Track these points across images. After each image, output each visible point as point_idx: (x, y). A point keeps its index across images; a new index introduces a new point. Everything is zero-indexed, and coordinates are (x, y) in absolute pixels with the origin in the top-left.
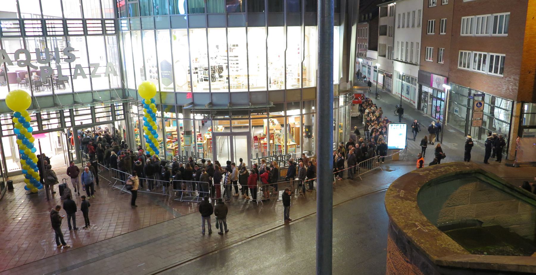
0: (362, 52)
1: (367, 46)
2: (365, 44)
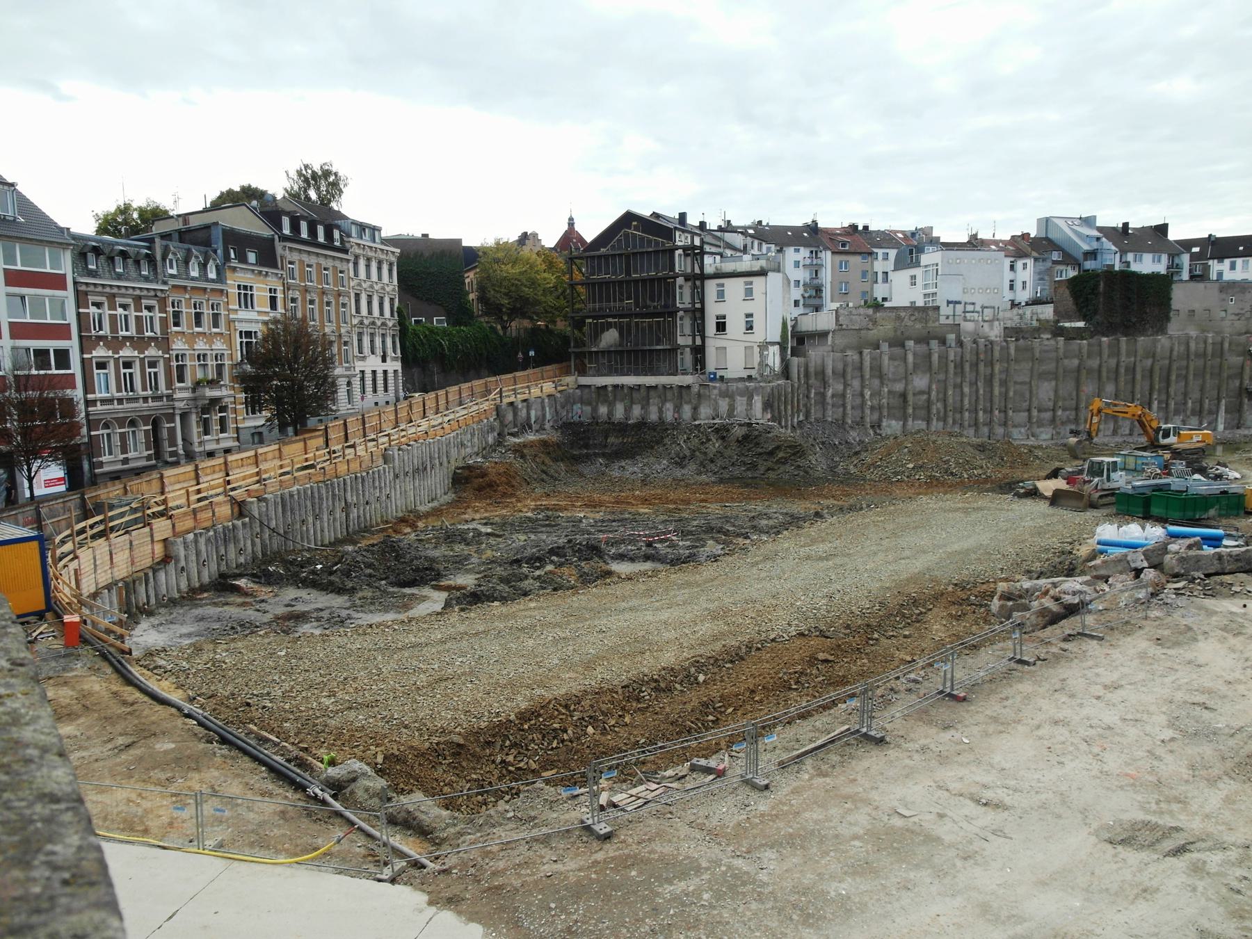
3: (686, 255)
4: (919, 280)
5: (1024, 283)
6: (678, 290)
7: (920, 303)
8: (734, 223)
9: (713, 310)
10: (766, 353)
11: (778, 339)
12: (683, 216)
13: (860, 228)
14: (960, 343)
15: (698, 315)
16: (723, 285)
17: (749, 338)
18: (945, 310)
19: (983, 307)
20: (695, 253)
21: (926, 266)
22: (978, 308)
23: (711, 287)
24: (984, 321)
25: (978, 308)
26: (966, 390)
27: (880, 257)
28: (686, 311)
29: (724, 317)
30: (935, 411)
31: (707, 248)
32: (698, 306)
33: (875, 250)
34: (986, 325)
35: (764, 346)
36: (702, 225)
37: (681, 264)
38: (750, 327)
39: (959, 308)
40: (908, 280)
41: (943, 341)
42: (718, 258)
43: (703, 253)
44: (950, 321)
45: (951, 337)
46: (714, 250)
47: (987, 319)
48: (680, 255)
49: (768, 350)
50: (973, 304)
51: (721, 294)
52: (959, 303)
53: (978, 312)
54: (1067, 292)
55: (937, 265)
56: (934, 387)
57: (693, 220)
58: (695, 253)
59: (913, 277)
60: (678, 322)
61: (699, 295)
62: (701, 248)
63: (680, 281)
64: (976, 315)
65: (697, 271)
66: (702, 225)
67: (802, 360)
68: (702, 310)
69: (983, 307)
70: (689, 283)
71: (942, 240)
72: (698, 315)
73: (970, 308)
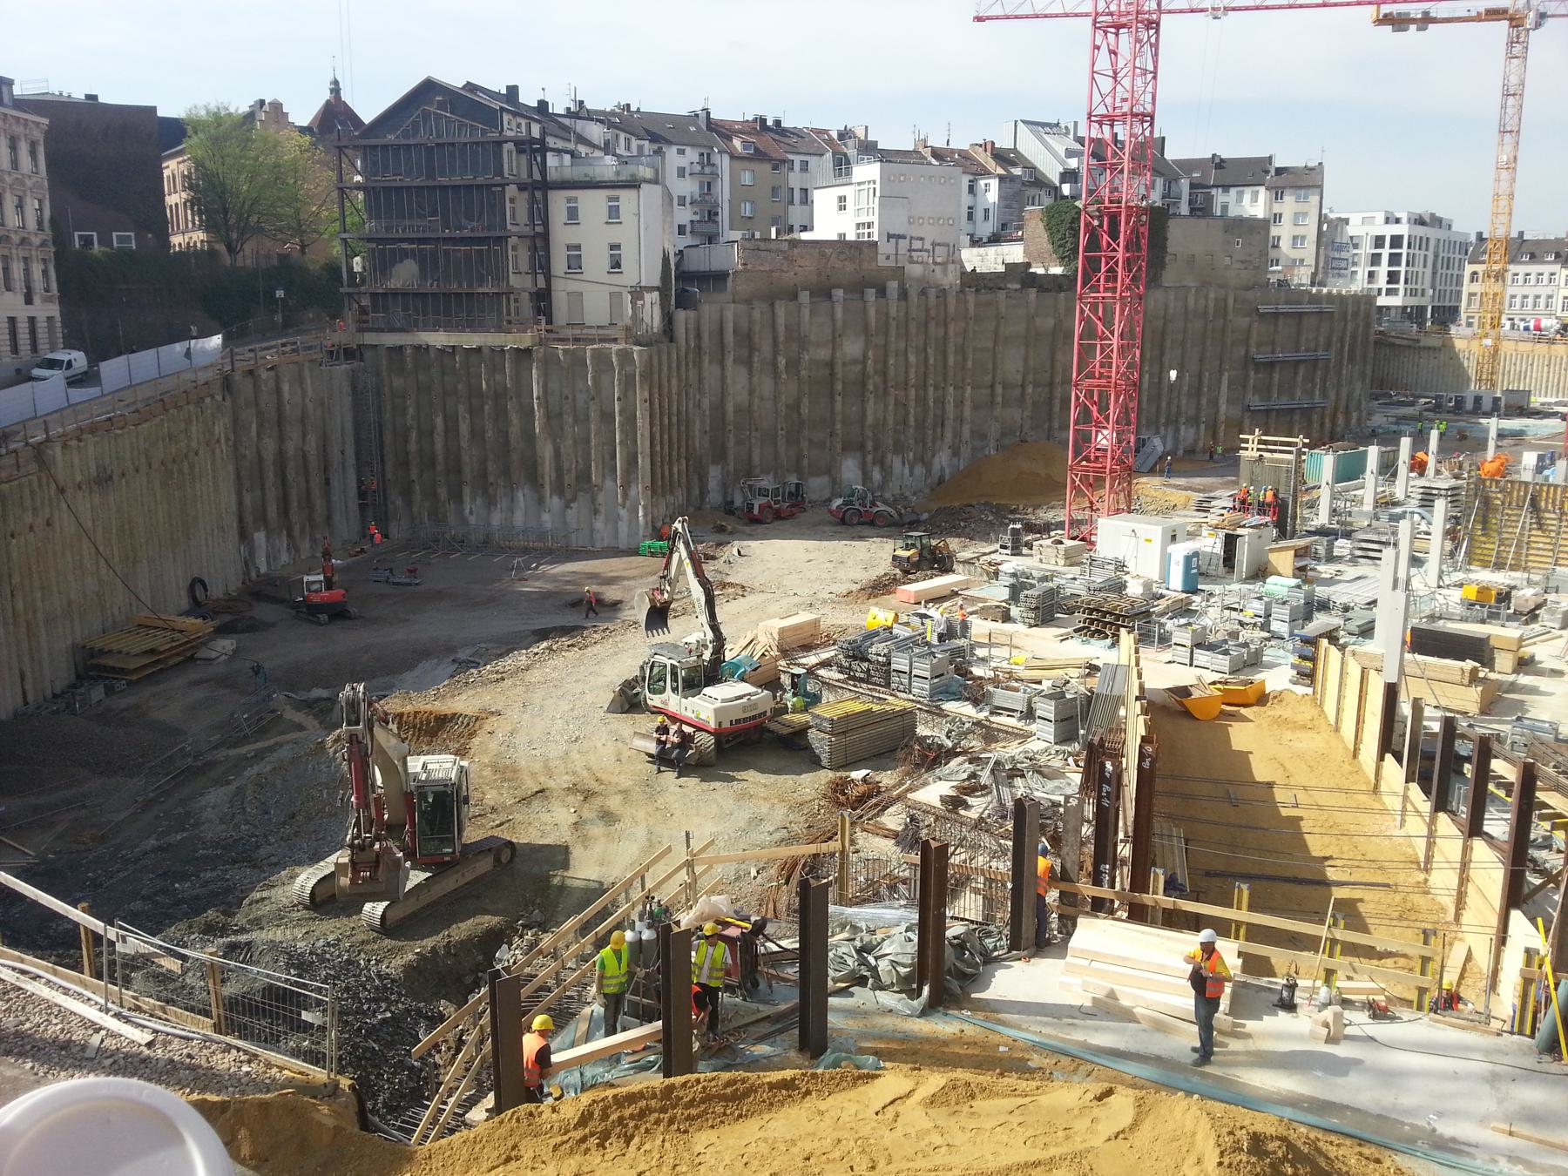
3: (520, 151)
4: (850, 203)
5: (987, 211)
6: (508, 205)
7: (851, 237)
8: (589, 105)
9: (562, 235)
10: (640, 303)
11: (657, 282)
12: (513, 91)
13: (770, 123)
14: (904, 294)
15: (539, 243)
16: (617, 199)
17: (615, 279)
18: (886, 248)
19: (934, 244)
20: (533, 149)
21: (859, 184)
22: (928, 246)
23: (558, 202)
24: (935, 263)
25: (928, 246)
26: (912, 358)
27: (797, 167)
29: (578, 247)
30: (871, 387)
31: (551, 142)
32: (539, 229)
33: (791, 157)
34: (938, 268)
35: (638, 293)
36: (543, 105)
37: (513, 164)
38: (616, 264)
39: (903, 244)
41: (882, 292)
42: (567, 157)
43: (544, 149)
45: (893, 285)
46: (560, 144)
47: (939, 260)
48: (510, 152)
49: (642, 298)
50: (922, 239)
51: (573, 214)
52: (904, 237)
53: (928, 251)
54: (1041, 225)
56: (870, 354)
57: (528, 98)
58: (533, 149)
59: (842, 199)
60: (510, 253)
61: (540, 214)
62: (542, 141)
63: (511, 191)
65: (537, 176)
66: (543, 105)
67: (692, 314)
68: (545, 236)
69: (934, 244)
70: (525, 195)
71: (1279, 163)
72: (539, 243)
73: (917, 245)
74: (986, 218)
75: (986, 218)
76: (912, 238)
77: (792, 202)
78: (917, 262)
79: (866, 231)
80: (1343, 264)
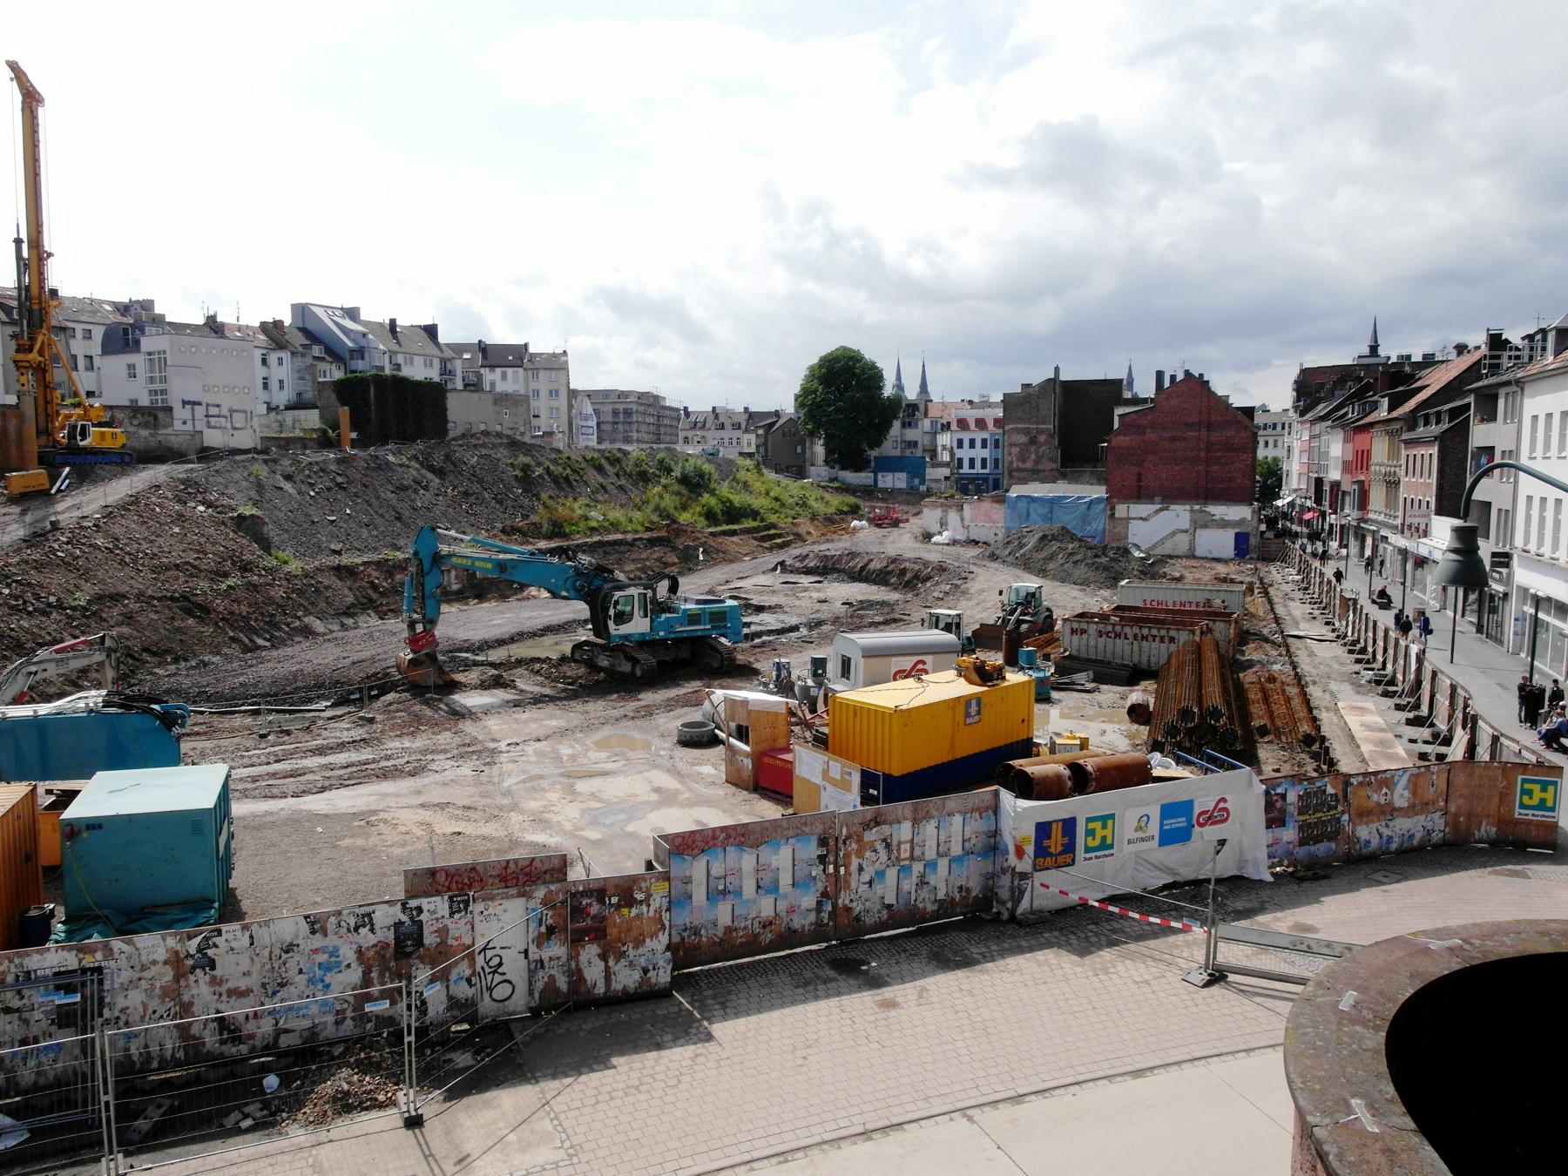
0: (1415, 521)
1: (1433, 506)
2: (1425, 496)
5: (281, 382)
7: (144, 401)
18: (180, 413)
22: (225, 412)
25: (225, 412)
27: (79, 334)
28: (876, 480)
40: (124, 371)
44: (189, 427)
50: (218, 406)
52: (199, 404)
53: (226, 417)
55: (164, 352)
59: (131, 367)
64: (223, 420)
69: (232, 411)
73: (214, 411)
74: (281, 388)
75: (281, 388)
76: (208, 405)
77: (76, 368)
78: (215, 427)
79: (159, 397)
80: (590, 431)
